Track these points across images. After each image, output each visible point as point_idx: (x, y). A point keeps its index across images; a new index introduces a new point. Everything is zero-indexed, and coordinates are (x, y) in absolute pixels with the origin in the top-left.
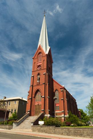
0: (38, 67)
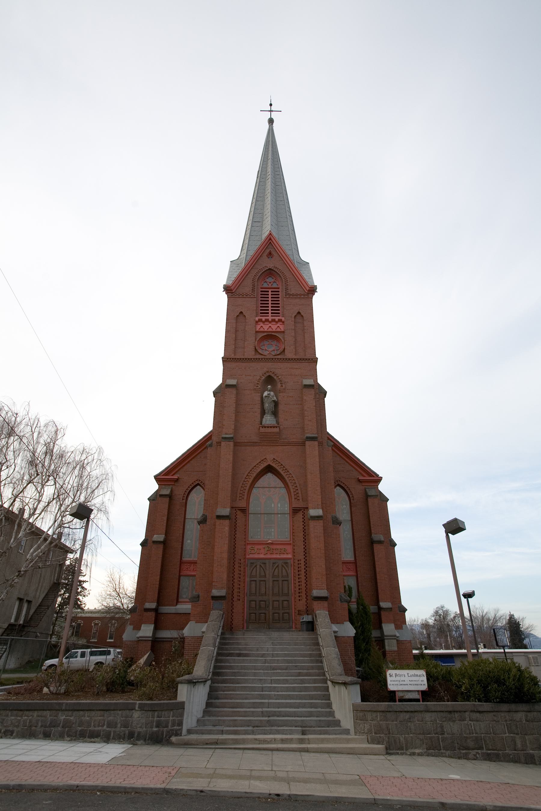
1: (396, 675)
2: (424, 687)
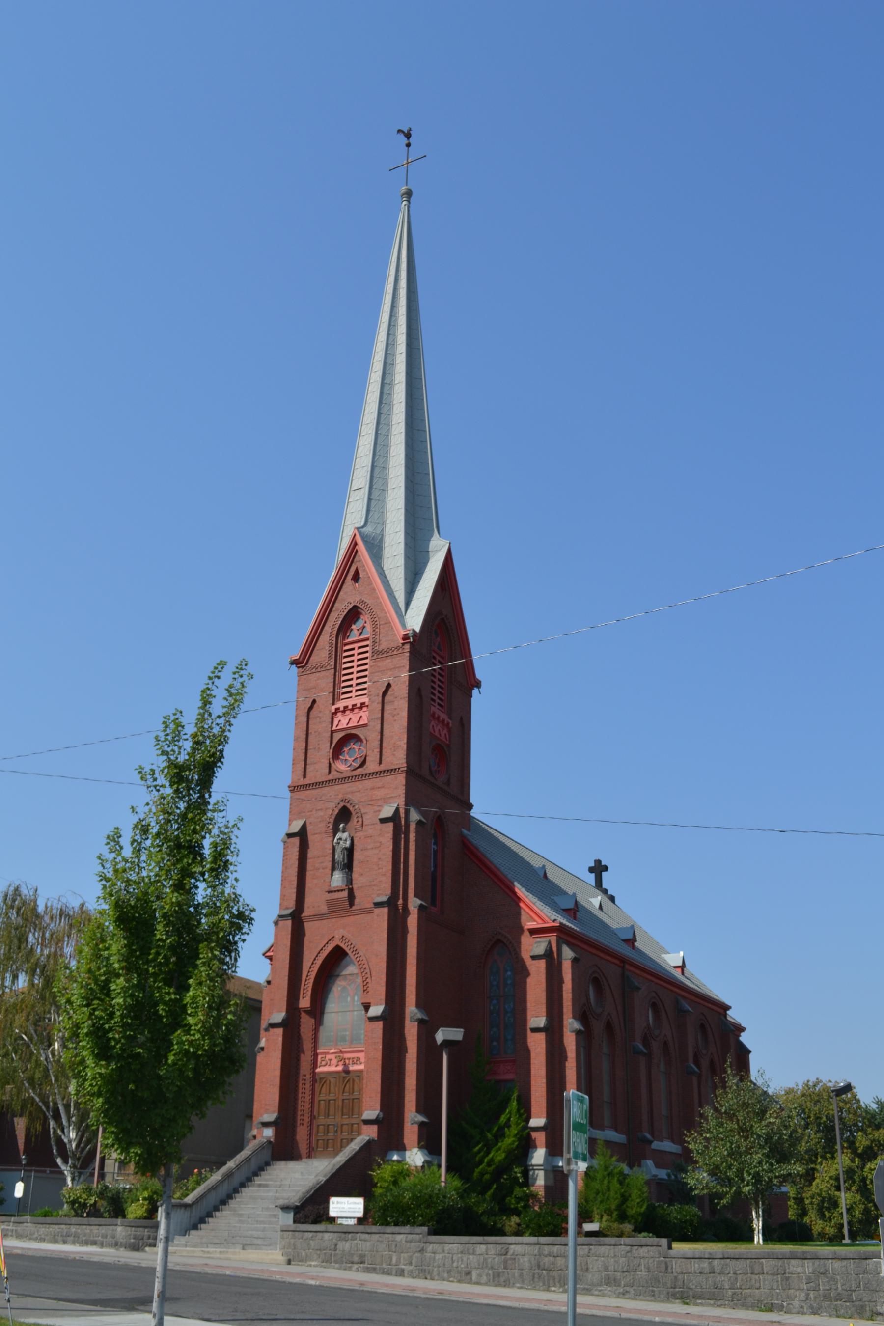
0: (338, 750)
1: (338, 1203)
2: (360, 1214)
